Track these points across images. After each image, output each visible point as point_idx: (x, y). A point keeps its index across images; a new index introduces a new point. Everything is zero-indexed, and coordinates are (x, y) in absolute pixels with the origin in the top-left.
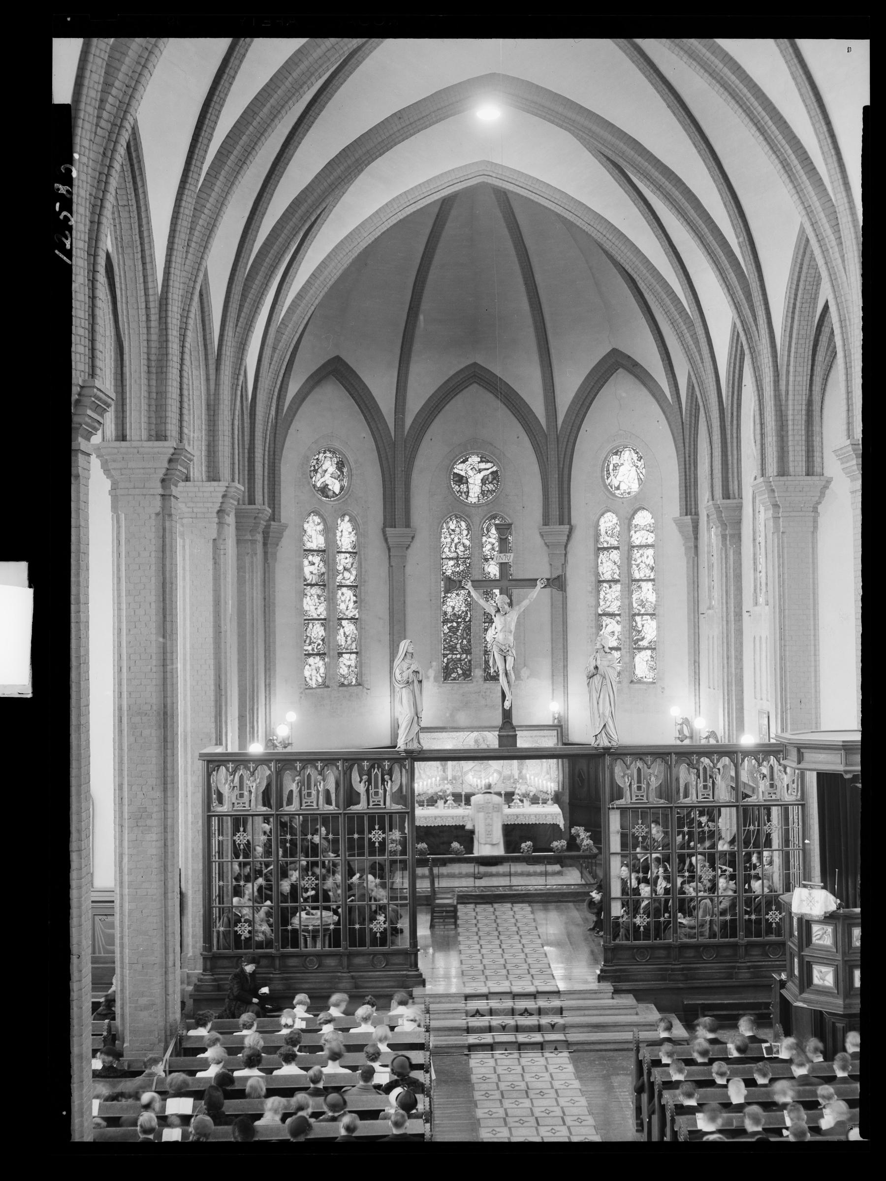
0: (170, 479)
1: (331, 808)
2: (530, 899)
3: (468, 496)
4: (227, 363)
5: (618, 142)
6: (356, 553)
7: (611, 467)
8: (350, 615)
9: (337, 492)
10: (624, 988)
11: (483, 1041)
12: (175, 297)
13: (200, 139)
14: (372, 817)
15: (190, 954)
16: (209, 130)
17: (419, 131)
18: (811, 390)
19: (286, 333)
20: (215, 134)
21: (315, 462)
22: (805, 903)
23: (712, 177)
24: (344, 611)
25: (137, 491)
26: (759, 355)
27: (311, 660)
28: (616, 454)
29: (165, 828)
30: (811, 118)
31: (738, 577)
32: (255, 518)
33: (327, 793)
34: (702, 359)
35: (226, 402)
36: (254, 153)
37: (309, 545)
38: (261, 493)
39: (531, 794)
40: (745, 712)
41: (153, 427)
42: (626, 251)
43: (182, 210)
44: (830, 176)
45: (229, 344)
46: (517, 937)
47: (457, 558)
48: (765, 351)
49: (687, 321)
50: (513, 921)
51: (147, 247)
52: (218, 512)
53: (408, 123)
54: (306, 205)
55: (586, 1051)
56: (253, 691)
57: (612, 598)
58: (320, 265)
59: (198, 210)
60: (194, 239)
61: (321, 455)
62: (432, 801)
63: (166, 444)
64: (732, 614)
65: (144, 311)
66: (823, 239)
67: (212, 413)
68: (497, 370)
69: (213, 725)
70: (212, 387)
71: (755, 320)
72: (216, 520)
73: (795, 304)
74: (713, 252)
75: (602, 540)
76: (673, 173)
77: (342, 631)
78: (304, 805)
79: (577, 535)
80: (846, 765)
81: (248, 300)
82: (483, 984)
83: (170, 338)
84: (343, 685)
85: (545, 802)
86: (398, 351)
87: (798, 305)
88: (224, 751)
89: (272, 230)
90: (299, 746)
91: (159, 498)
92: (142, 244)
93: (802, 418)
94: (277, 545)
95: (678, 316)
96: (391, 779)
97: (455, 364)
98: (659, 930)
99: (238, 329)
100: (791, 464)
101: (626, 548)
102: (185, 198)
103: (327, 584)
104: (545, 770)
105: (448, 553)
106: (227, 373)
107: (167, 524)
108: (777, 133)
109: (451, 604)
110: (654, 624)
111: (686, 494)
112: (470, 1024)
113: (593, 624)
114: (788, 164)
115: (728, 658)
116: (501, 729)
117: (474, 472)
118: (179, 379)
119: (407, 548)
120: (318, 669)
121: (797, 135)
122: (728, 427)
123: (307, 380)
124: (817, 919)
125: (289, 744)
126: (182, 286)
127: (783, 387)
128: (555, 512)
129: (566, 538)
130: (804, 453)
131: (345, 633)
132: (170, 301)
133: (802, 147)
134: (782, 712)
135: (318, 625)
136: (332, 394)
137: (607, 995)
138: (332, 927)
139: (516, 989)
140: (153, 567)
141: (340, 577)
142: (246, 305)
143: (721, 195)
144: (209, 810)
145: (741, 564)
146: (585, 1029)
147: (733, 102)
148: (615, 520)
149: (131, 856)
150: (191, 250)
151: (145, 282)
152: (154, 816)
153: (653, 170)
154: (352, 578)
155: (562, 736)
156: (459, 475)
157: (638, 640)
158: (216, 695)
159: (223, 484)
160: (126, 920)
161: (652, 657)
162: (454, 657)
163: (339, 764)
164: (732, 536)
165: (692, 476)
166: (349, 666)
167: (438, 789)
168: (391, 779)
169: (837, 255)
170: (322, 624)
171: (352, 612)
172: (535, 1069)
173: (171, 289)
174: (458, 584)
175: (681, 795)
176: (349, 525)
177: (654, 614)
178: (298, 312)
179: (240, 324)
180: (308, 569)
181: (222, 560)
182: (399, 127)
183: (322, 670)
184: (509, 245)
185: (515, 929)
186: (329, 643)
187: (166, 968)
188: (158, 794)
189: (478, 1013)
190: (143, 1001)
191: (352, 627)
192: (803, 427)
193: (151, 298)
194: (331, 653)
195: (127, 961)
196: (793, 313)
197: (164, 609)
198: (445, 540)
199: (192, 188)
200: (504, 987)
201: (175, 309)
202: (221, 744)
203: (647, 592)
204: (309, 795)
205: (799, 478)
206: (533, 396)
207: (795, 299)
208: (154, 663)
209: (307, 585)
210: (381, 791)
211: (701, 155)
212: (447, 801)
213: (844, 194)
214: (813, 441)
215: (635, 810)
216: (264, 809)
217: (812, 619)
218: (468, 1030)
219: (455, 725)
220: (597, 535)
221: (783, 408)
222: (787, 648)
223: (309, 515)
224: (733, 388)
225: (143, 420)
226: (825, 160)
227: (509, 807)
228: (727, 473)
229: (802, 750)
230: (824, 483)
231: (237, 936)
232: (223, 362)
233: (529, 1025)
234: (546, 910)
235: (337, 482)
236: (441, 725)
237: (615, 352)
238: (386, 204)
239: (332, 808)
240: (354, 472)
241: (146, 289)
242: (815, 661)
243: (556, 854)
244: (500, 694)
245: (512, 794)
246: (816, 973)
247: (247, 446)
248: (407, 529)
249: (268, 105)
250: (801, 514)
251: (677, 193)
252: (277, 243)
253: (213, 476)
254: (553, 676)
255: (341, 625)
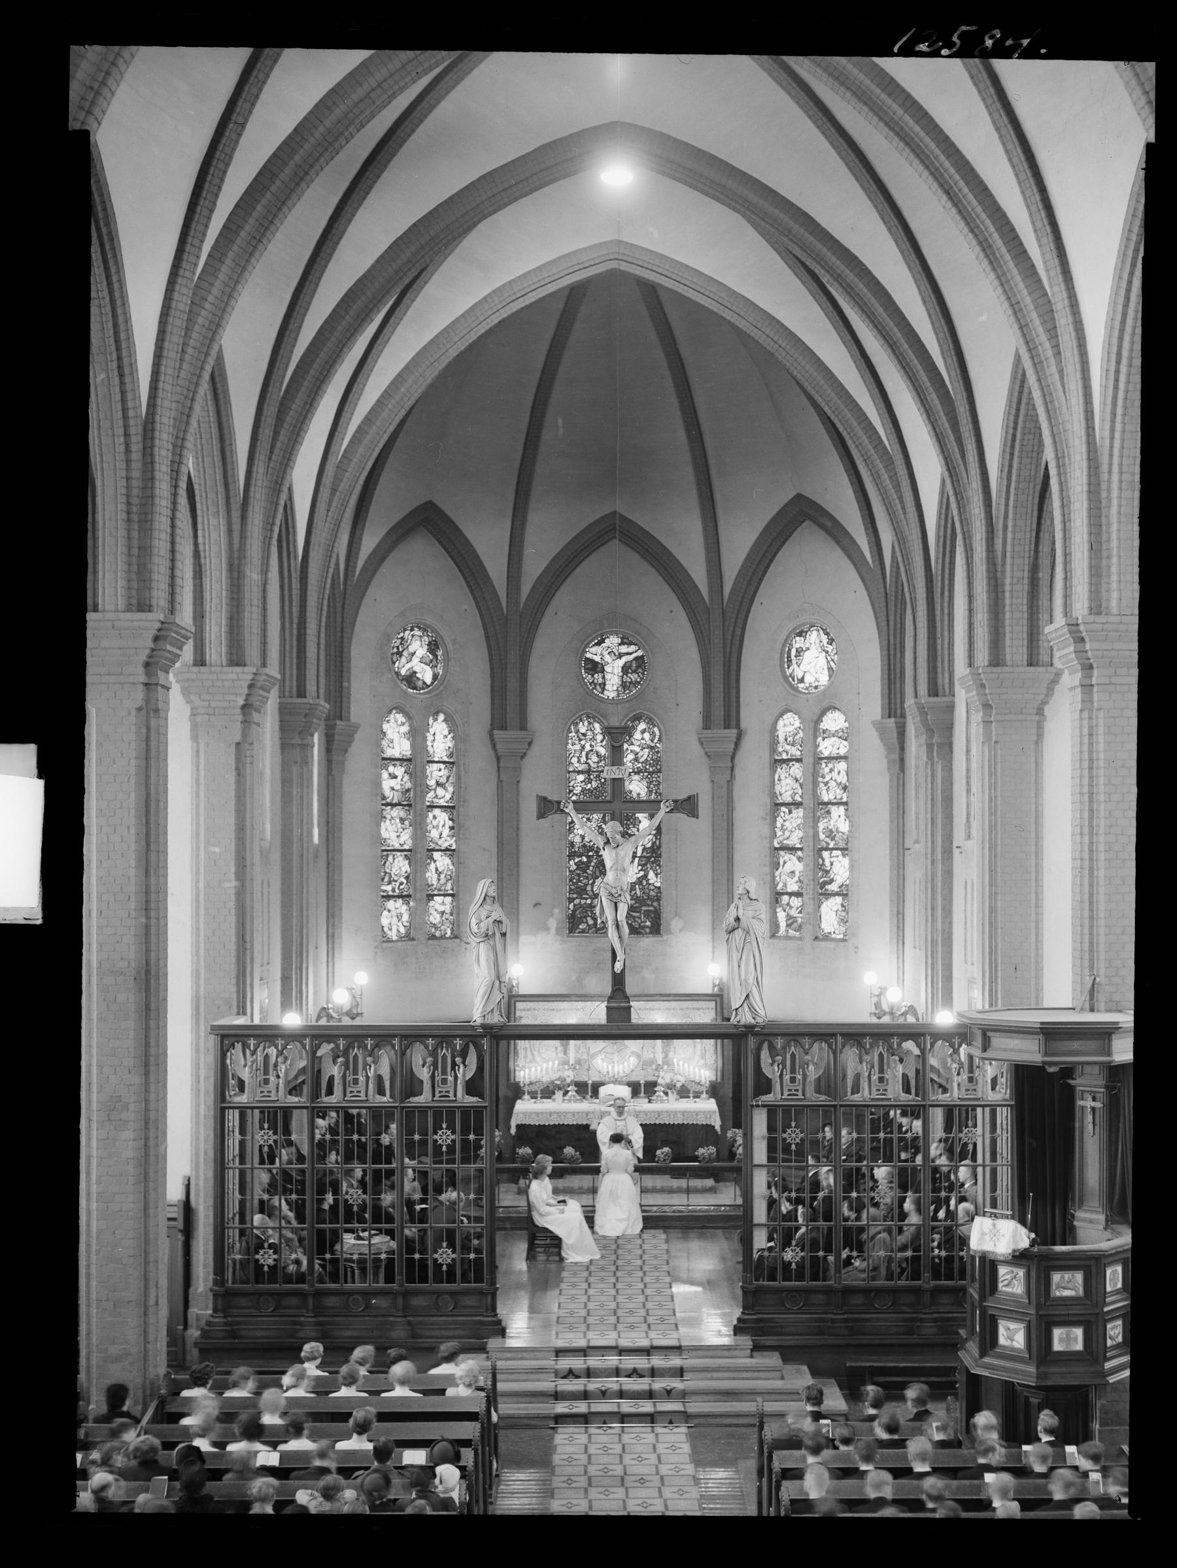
0: (157, 663)
1: (384, 1099)
2: (666, 1224)
3: (603, 689)
4: (257, 509)
5: (782, 216)
6: (453, 763)
7: (793, 652)
8: (445, 845)
9: (428, 681)
10: (768, 1343)
11: (575, 1411)
12: (165, 420)
13: (198, 210)
14: (438, 1113)
15: (201, 1289)
16: (210, 197)
17: (516, 199)
18: (1037, 551)
19: (350, 470)
20: (219, 203)
21: (399, 641)
22: (987, 1237)
23: (907, 264)
24: (436, 839)
25: (113, 679)
26: (969, 503)
27: (391, 904)
28: (800, 634)
29: (147, 1123)
30: (1019, 182)
31: (948, 800)
32: (306, 715)
33: (379, 1079)
34: (903, 508)
35: (255, 561)
36: (272, 228)
37: (389, 753)
38: (314, 683)
39: (679, 1085)
40: (954, 980)
41: (134, 593)
42: (804, 362)
43: (174, 304)
44: (1045, 262)
45: (259, 483)
46: (640, 1274)
47: (588, 772)
48: (976, 499)
49: (885, 458)
50: (639, 1252)
51: (124, 353)
52: (243, 707)
53: (501, 188)
54: (363, 298)
55: (710, 1425)
56: (302, 944)
57: (791, 826)
58: (395, 379)
59: (196, 305)
60: (192, 342)
61: (407, 632)
62: (548, 1092)
63: (150, 616)
64: (939, 850)
65: (122, 439)
66: (1036, 347)
67: (236, 575)
68: (643, 520)
69: (234, 989)
70: (236, 541)
71: (963, 457)
72: (240, 718)
73: (1014, 436)
74: (908, 364)
75: (780, 749)
76: (856, 257)
77: (433, 866)
78: (349, 1095)
79: (748, 743)
80: (1046, 1054)
81: (286, 425)
82: (582, 1335)
83: (157, 475)
84: (433, 937)
85: (697, 1095)
86: (511, 496)
87: (1019, 436)
88: (249, 1023)
89: (319, 332)
90: (372, 1017)
91: (141, 687)
92: (118, 349)
93: (1024, 588)
94: (346, 751)
95: (872, 451)
96: (464, 1062)
97: (588, 514)
98: (816, 1269)
99: (272, 464)
100: (1008, 650)
101: (811, 760)
102: (177, 287)
103: (414, 804)
104: (698, 1053)
105: (577, 765)
106: (256, 522)
107: (153, 723)
108: (975, 203)
109: (581, 832)
110: (846, 862)
111: (889, 689)
112: (559, 1388)
113: (767, 861)
114: (990, 246)
115: (933, 909)
116: (611, 998)
117: (612, 658)
118: (169, 530)
119: (522, 757)
120: (399, 917)
121: (1002, 206)
122: (938, 600)
123: (388, 533)
124: (1002, 1258)
125: (358, 1014)
126: (174, 405)
127: (998, 546)
128: (718, 712)
129: (733, 746)
130: (1025, 636)
131: (437, 869)
132: (158, 426)
133: (1008, 223)
134: (991, 982)
135: (401, 858)
136: (422, 551)
137: (742, 1353)
138: (383, 1256)
139: (624, 1343)
140: (133, 780)
141: (431, 795)
142: (283, 431)
143: (918, 287)
144: (223, 1098)
145: (952, 784)
146: (711, 1398)
147: (916, 161)
148: (797, 724)
149: (100, 1158)
150: (187, 358)
151: (123, 400)
152: (132, 1107)
153: (829, 254)
154: (448, 796)
155: (722, 1008)
156: (592, 661)
157: (826, 883)
158: (238, 950)
159: (250, 670)
160: (94, 1242)
161: (843, 906)
162: (583, 902)
163: (396, 1041)
164: (940, 746)
165: (898, 665)
166: (443, 913)
167: (556, 1076)
168: (464, 1062)
169: (1054, 369)
170: (406, 857)
171: (448, 842)
172: (639, 1448)
173: (159, 410)
174: (556, 805)
175: (323, 1092)
176: (444, 725)
177: (847, 849)
178: (365, 441)
179: (274, 457)
180: (387, 784)
181: (248, 771)
182: (490, 194)
183: (405, 918)
184: (659, 354)
185: (639, 1262)
186: (415, 882)
187: (146, 1307)
188: (137, 1080)
189: (571, 1374)
190: (114, 1350)
191: (447, 861)
192: (1025, 601)
193: (132, 422)
194: (418, 895)
195: (94, 1296)
196: (1013, 447)
197: (148, 835)
198: (574, 748)
199: (187, 274)
200: (609, 1339)
201: (165, 436)
202: (244, 1014)
203: (838, 820)
204: (356, 1081)
205: (1016, 669)
206: (692, 558)
207: (1015, 429)
208: (133, 905)
209: (387, 804)
210: (450, 1078)
211: (891, 234)
212: (567, 1092)
213: (1063, 286)
214: (1038, 619)
215: (787, 1109)
216: (904, 1097)
217: (1033, 857)
218: (557, 1396)
219: (582, 992)
220: (774, 742)
221: (999, 574)
222: (999, 897)
223: (390, 712)
224: (944, 548)
225: (120, 584)
226: (1038, 240)
227: (649, 1102)
228: (935, 660)
229: (989, 1034)
230: (1052, 676)
231: (258, 1267)
232: (251, 508)
233: (652, 1387)
234: (685, 1238)
235: (428, 668)
236: (563, 991)
237: (799, 497)
238: (485, 298)
239: (385, 1100)
240: (451, 655)
241: (125, 410)
242: (1037, 914)
243: (702, 1164)
244: (610, 954)
245: (655, 1084)
246: (1002, 1331)
247: (296, 621)
248: (523, 732)
249: (292, 164)
250: (1021, 717)
251: (861, 285)
252: (325, 349)
253: (236, 659)
254: (714, 929)
255: (432, 858)
